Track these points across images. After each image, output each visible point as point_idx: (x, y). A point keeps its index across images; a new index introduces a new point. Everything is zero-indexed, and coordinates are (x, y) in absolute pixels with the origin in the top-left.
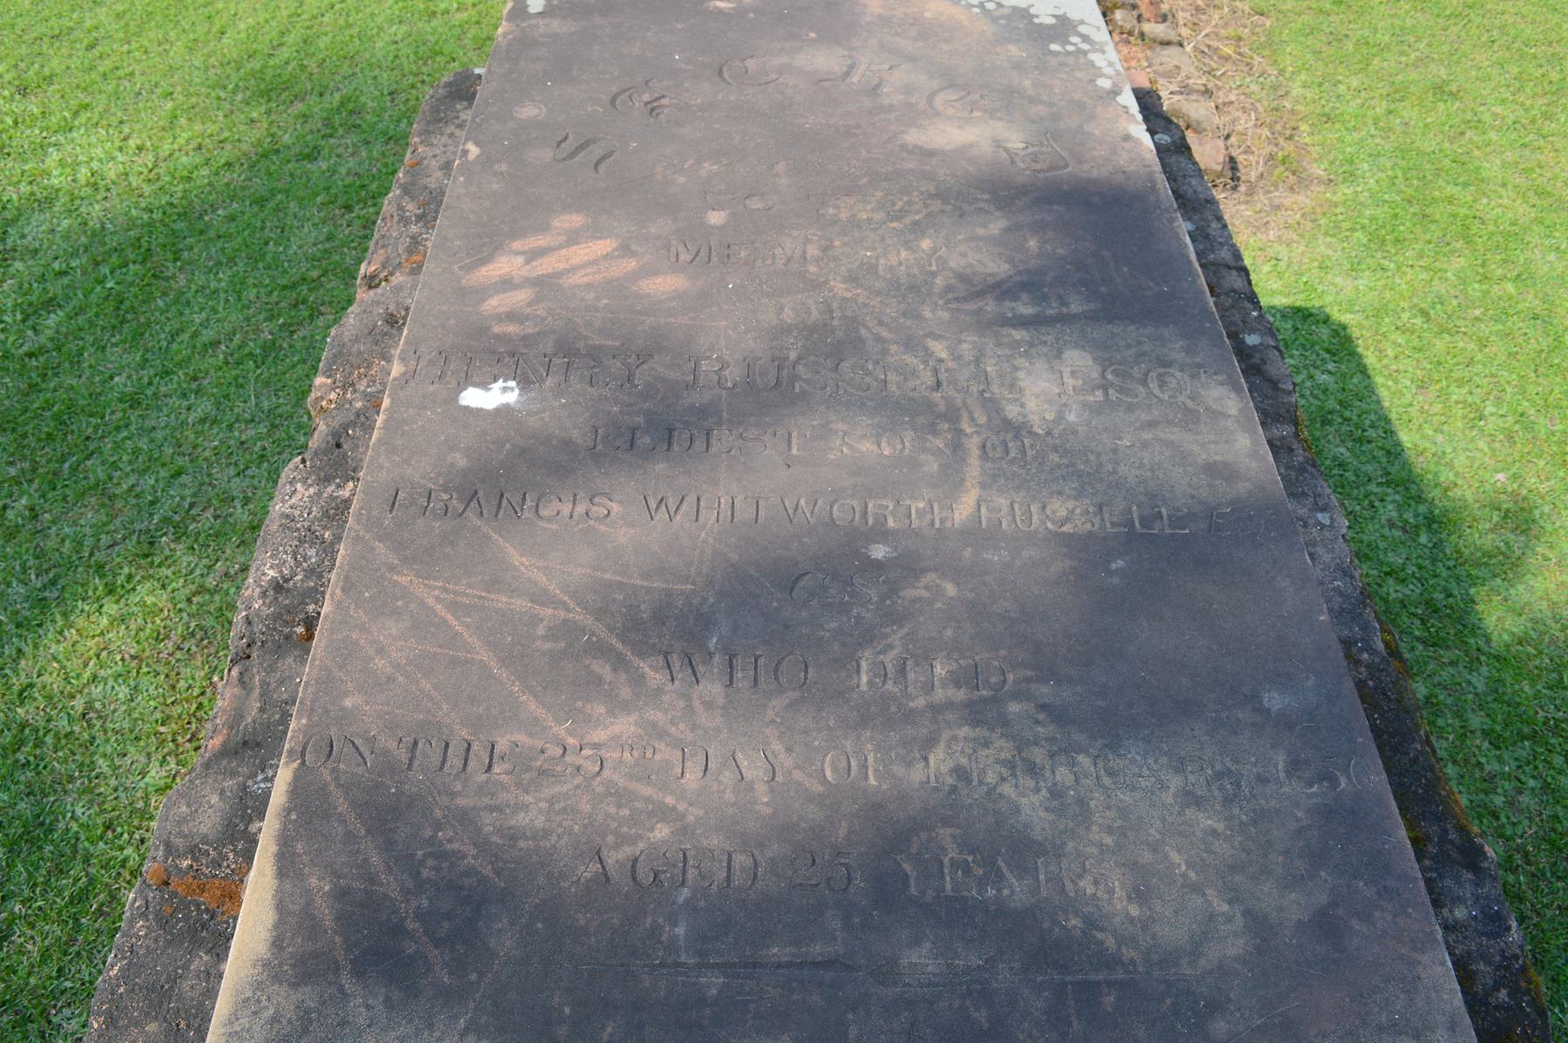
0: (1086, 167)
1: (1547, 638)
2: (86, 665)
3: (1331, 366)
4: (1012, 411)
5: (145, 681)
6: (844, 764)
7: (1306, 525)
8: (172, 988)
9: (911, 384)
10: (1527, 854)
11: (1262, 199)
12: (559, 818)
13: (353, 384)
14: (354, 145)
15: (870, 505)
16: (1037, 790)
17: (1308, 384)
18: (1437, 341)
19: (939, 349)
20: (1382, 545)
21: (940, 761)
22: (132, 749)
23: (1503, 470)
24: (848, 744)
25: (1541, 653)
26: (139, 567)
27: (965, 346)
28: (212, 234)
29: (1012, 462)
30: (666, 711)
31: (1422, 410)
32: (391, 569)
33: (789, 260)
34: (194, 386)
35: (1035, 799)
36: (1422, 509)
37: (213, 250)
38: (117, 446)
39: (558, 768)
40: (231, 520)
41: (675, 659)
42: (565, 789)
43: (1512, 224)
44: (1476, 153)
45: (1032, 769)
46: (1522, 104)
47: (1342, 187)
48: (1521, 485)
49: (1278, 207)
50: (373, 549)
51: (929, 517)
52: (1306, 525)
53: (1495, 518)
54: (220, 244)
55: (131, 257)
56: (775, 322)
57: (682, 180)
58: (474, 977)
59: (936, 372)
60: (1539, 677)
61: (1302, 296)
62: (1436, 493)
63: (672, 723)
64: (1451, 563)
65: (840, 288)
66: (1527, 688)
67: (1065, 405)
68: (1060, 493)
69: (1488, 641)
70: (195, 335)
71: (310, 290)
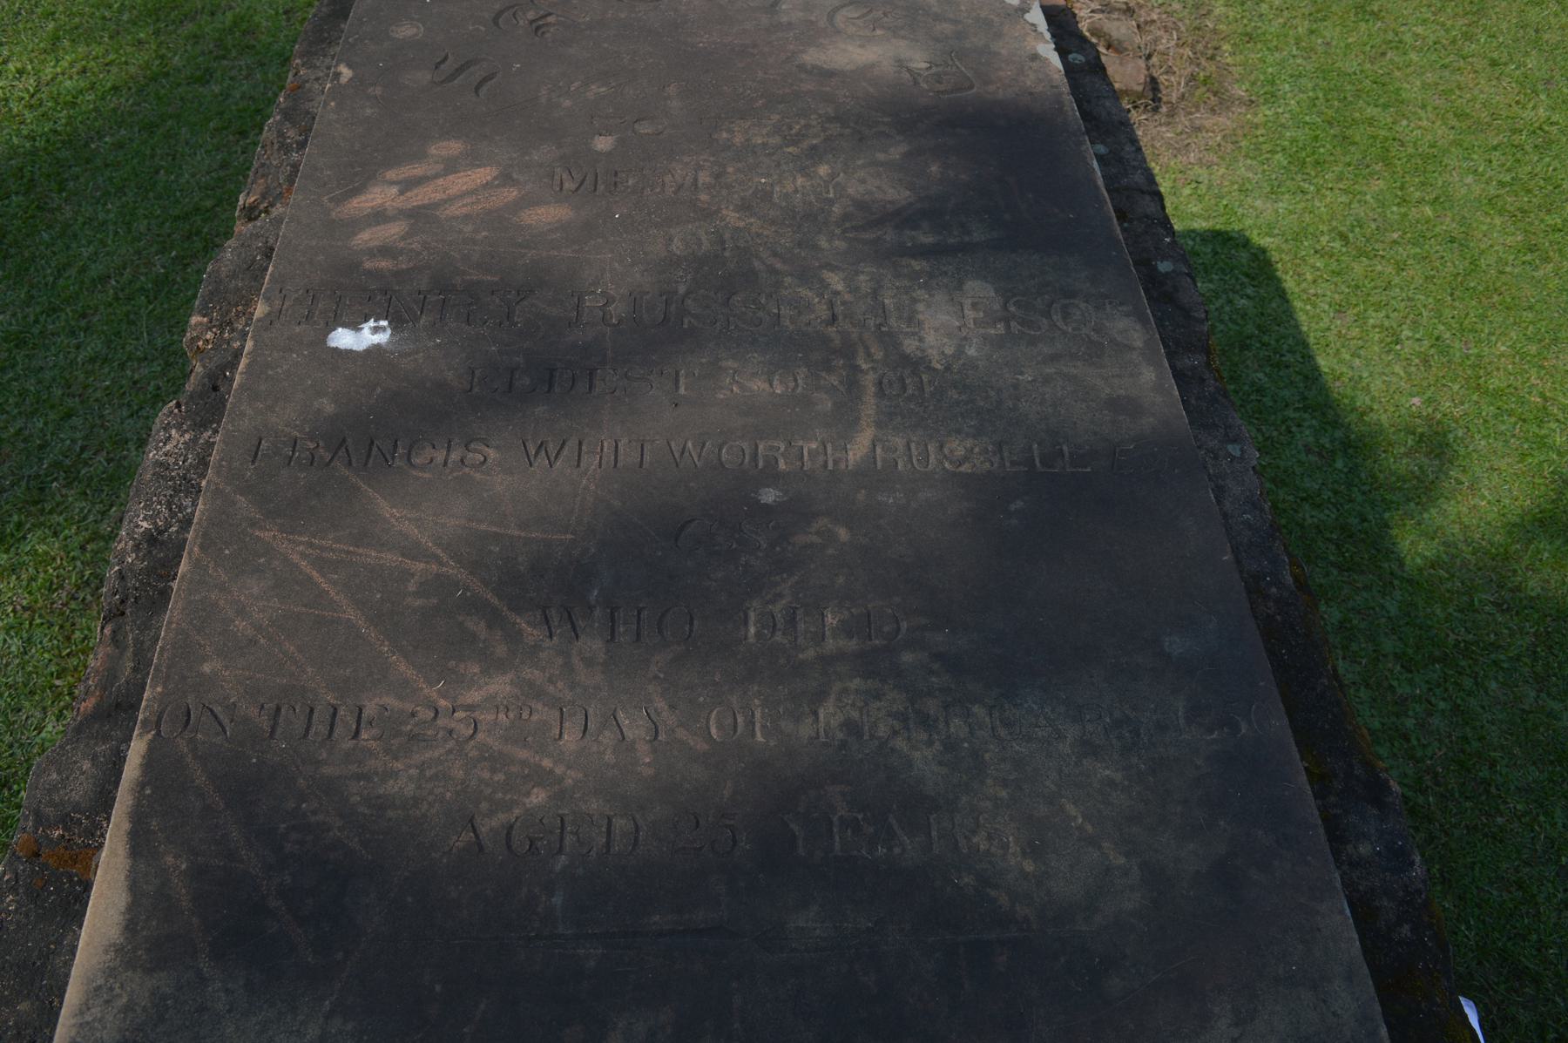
0: (991, 88)
1: (1458, 561)
3: (1249, 291)
4: (910, 345)
5: (38, 633)
6: (730, 721)
7: (1216, 458)
10: (1436, 775)
11: (1182, 121)
12: (429, 786)
13: (230, 323)
14: (248, 67)
15: (761, 447)
16: (930, 743)
17: (1227, 309)
19: (836, 281)
20: (1298, 470)
21: (830, 715)
22: (27, 704)
23: (1418, 394)
24: (734, 699)
26: (29, 514)
27: (862, 277)
28: (99, 162)
30: (543, 670)
32: (253, 524)
33: (680, 187)
34: (83, 323)
36: (1338, 434)
37: (100, 179)
39: (429, 733)
42: (436, 754)
43: (1431, 146)
44: (1397, 74)
45: (926, 721)
46: (1443, 25)
48: (1435, 410)
49: (1199, 129)
51: (821, 458)
52: (1216, 458)
54: (107, 173)
55: (13, 188)
57: (567, 103)
58: (340, 956)
59: (831, 305)
61: (1222, 220)
62: (1353, 417)
63: (550, 681)
64: (1367, 488)
65: (732, 216)
66: (1438, 612)
67: (965, 338)
68: (958, 432)
69: (1402, 565)
70: (83, 270)
71: (205, 221)
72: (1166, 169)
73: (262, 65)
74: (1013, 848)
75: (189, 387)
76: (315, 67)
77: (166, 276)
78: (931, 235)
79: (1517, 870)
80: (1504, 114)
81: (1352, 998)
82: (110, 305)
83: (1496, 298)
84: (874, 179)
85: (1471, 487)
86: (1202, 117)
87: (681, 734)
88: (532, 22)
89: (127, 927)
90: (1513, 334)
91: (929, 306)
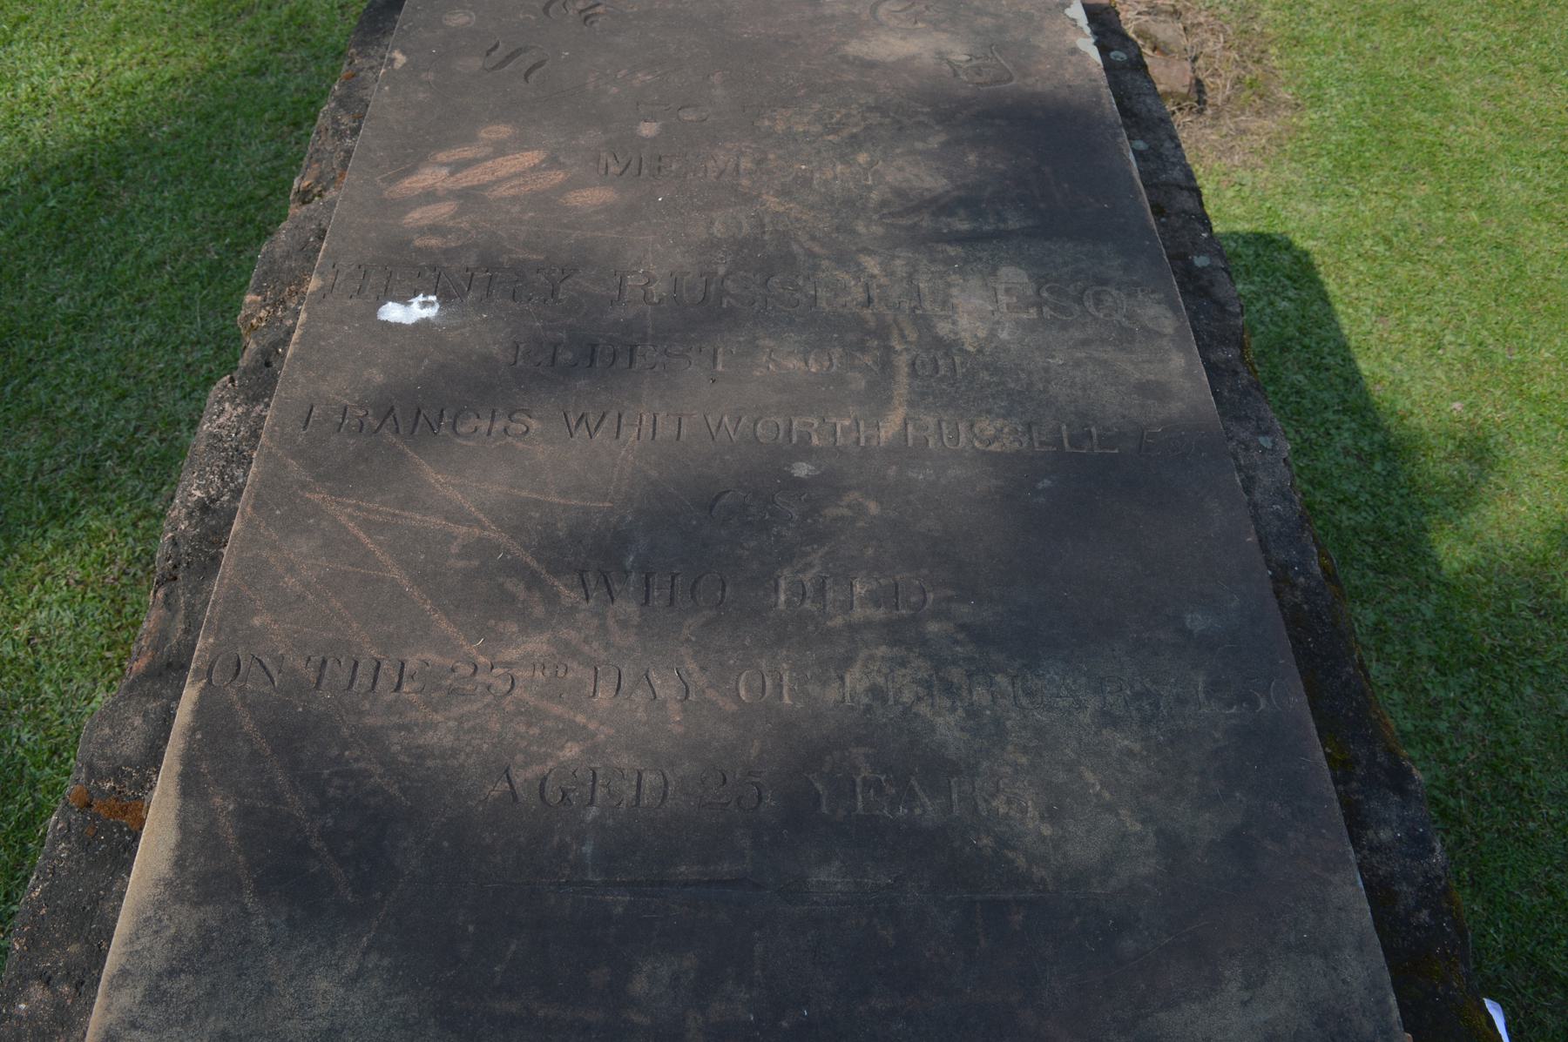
0: (1030, 81)
1: (1496, 567)
2: (30, 590)
3: (1291, 293)
4: (943, 328)
5: (90, 607)
6: (758, 683)
7: (1247, 449)
8: (93, 910)
9: (841, 300)
10: (1468, 778)
11: (1227, 124)
12: (468, 737)
13: (283, 302)
15: (795, 424)
16: (953, 710)
17: (1268, 310)
18: (1399, 269)
19: (872, 265)
20: (1336, 472)
21: (856, 680)
22: (78, 675)
24: (763, 663)
25: (1490, 581)
26: (84, 491)
27: (898, 262)
28: (156, 151)
29: (942, 380)
30: (579, 630)
31: (1381, 339)
32: (304, 486)
33: (722, 173)
34: (138, 307)
35: (951, 719)
36: (1378, 437)
37: (158, 168)
38: (61, 369)
40: (177, 444)
41: (591, 578)
42: (475, 708)
43: (1478, 152)
44: (1446, 79)
45: (949, 689)
47: (1310, 112)
48: (1476, 415)
49: (1244, 132)
50: (285, 466)
51: (854, 435)
52: (1247, 449)
53: (1450, 447)
54: (165, 162)
56: (704, 237)
57: (614, 90)
58: (378, 895)
59: (867, 288)
60: (1488, 604)
61: (1265, 222)
62: (1392, 421)
63: (586, 641)
64: (1405, 491)
66: (1474, 616)
67: (998, 322)
68: (989, 412)
69: (1439, 568)
70: (140, 255)
71: (258, 209)
72: (1210, 171)
73: (317, 58)
74: (1031, 812)
75: (242, 363)
76: (369, 56)
77: (220, 262)
78: (968, 226)
79: (1548, 876)
80: (1554, 120)
81: (1363, 973)
82: (166, 289)
83: (1541, 304)
84: (915, 170)
85: (1511, 493)
86: (1247, 120)
87: (711, 694)
88: (581, 12)
89: (176, 863)
90: (1557, 341)
91: (963, 290)
